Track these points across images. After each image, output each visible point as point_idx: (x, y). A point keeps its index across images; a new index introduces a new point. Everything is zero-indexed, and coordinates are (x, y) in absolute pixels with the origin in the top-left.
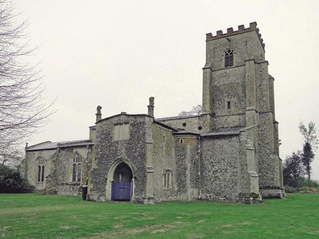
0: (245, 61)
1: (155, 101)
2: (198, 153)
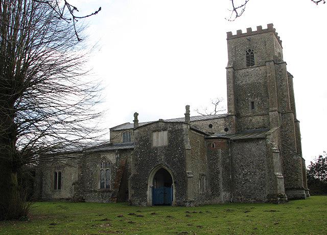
2: (229, 157)
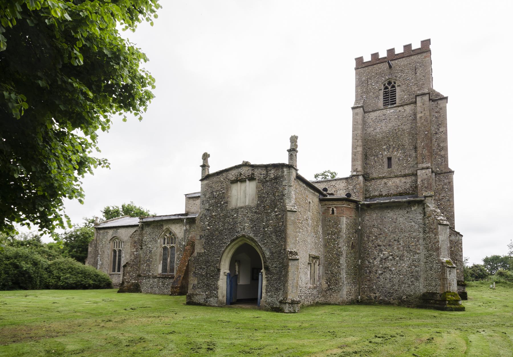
0: (416, 96)
1: (299, 142)
